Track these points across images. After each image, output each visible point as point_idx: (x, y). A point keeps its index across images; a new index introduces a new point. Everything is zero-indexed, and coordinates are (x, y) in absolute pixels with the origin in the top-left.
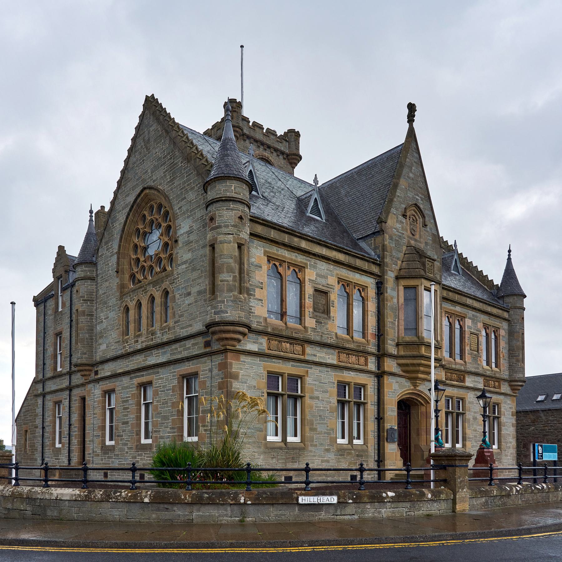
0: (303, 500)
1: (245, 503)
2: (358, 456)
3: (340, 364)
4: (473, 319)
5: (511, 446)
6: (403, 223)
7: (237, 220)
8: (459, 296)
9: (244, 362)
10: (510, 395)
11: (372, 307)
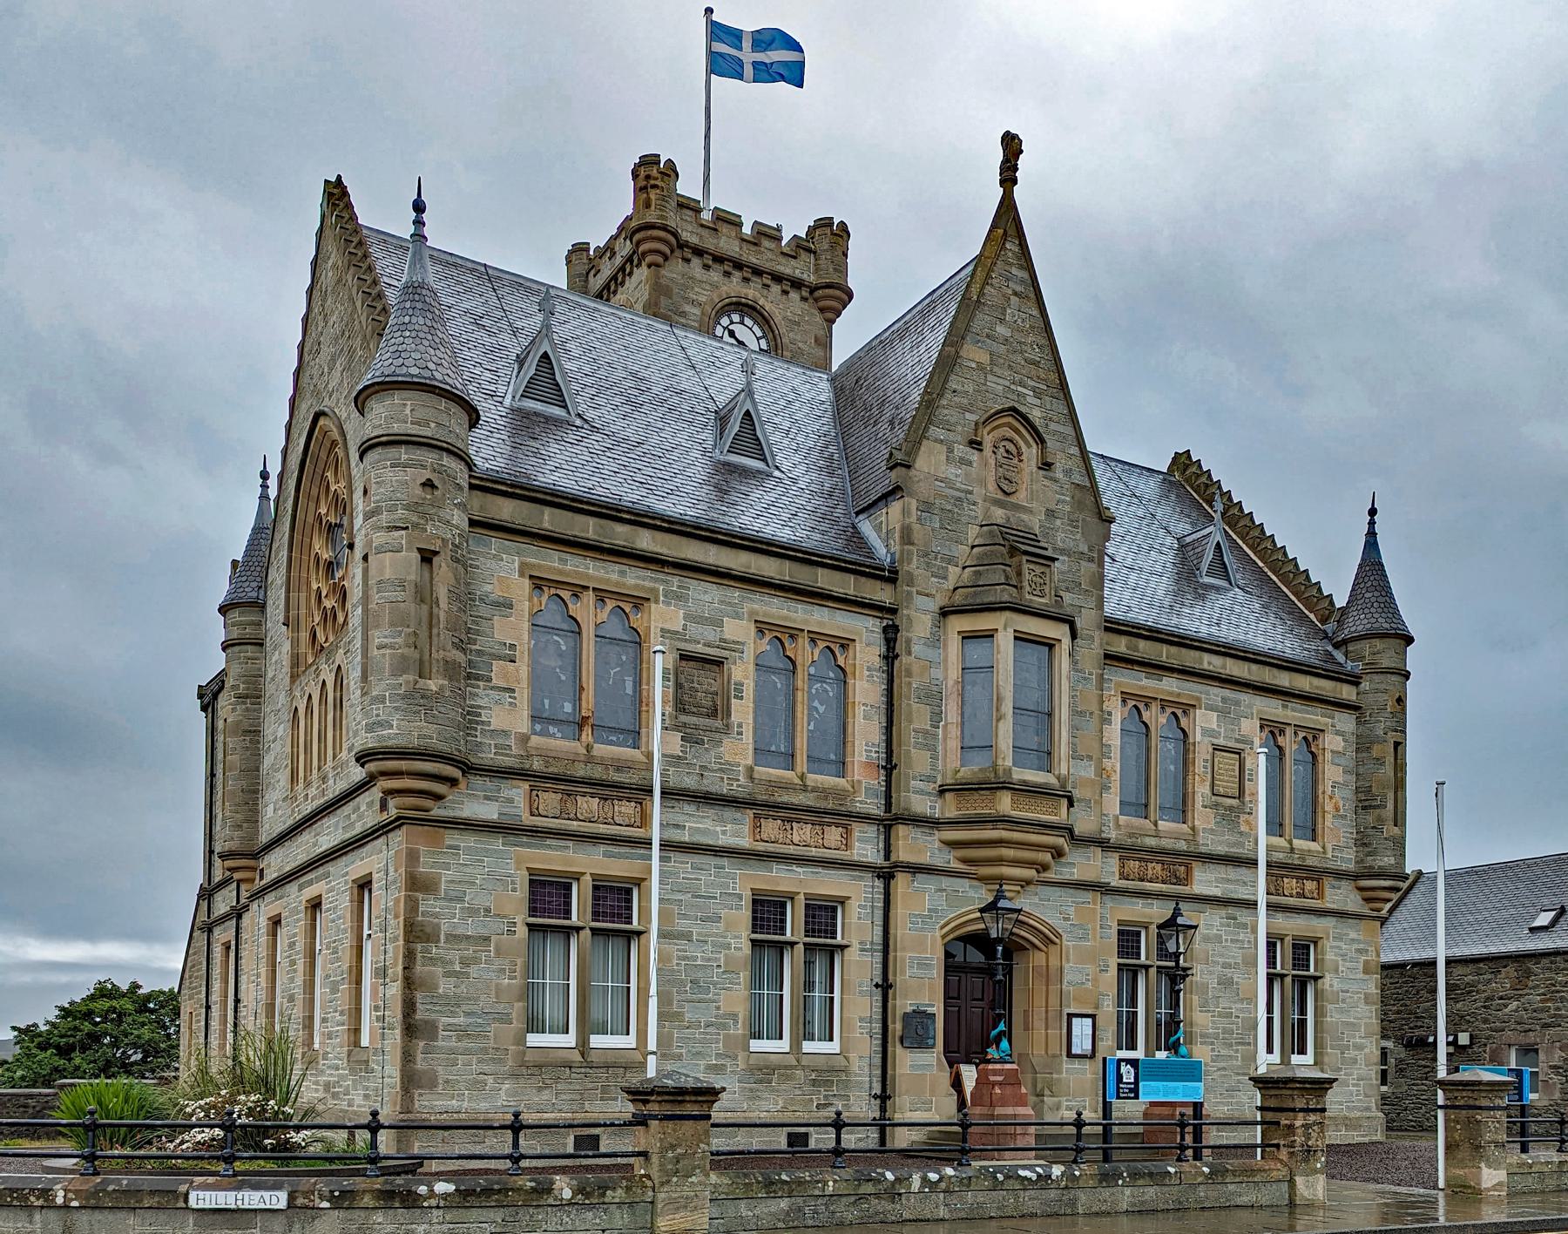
0: (201, 1199)
1: (66, 1207)
2: (814, 1082)
3: (761, 847)
4: (1223, 713)
5: (1361, 1057)
6: (970, 464)
7: (419, 491)
8: (1174, 649)
9: (457, 848)
10: (1359, 917)
11: (866, 691)
